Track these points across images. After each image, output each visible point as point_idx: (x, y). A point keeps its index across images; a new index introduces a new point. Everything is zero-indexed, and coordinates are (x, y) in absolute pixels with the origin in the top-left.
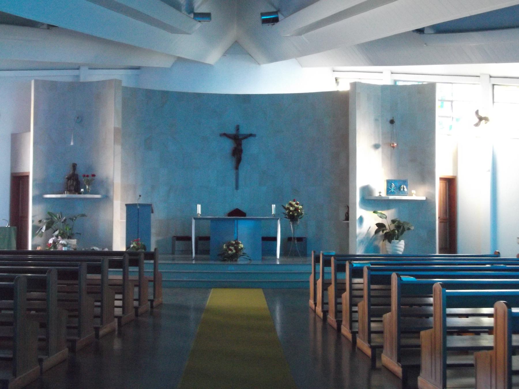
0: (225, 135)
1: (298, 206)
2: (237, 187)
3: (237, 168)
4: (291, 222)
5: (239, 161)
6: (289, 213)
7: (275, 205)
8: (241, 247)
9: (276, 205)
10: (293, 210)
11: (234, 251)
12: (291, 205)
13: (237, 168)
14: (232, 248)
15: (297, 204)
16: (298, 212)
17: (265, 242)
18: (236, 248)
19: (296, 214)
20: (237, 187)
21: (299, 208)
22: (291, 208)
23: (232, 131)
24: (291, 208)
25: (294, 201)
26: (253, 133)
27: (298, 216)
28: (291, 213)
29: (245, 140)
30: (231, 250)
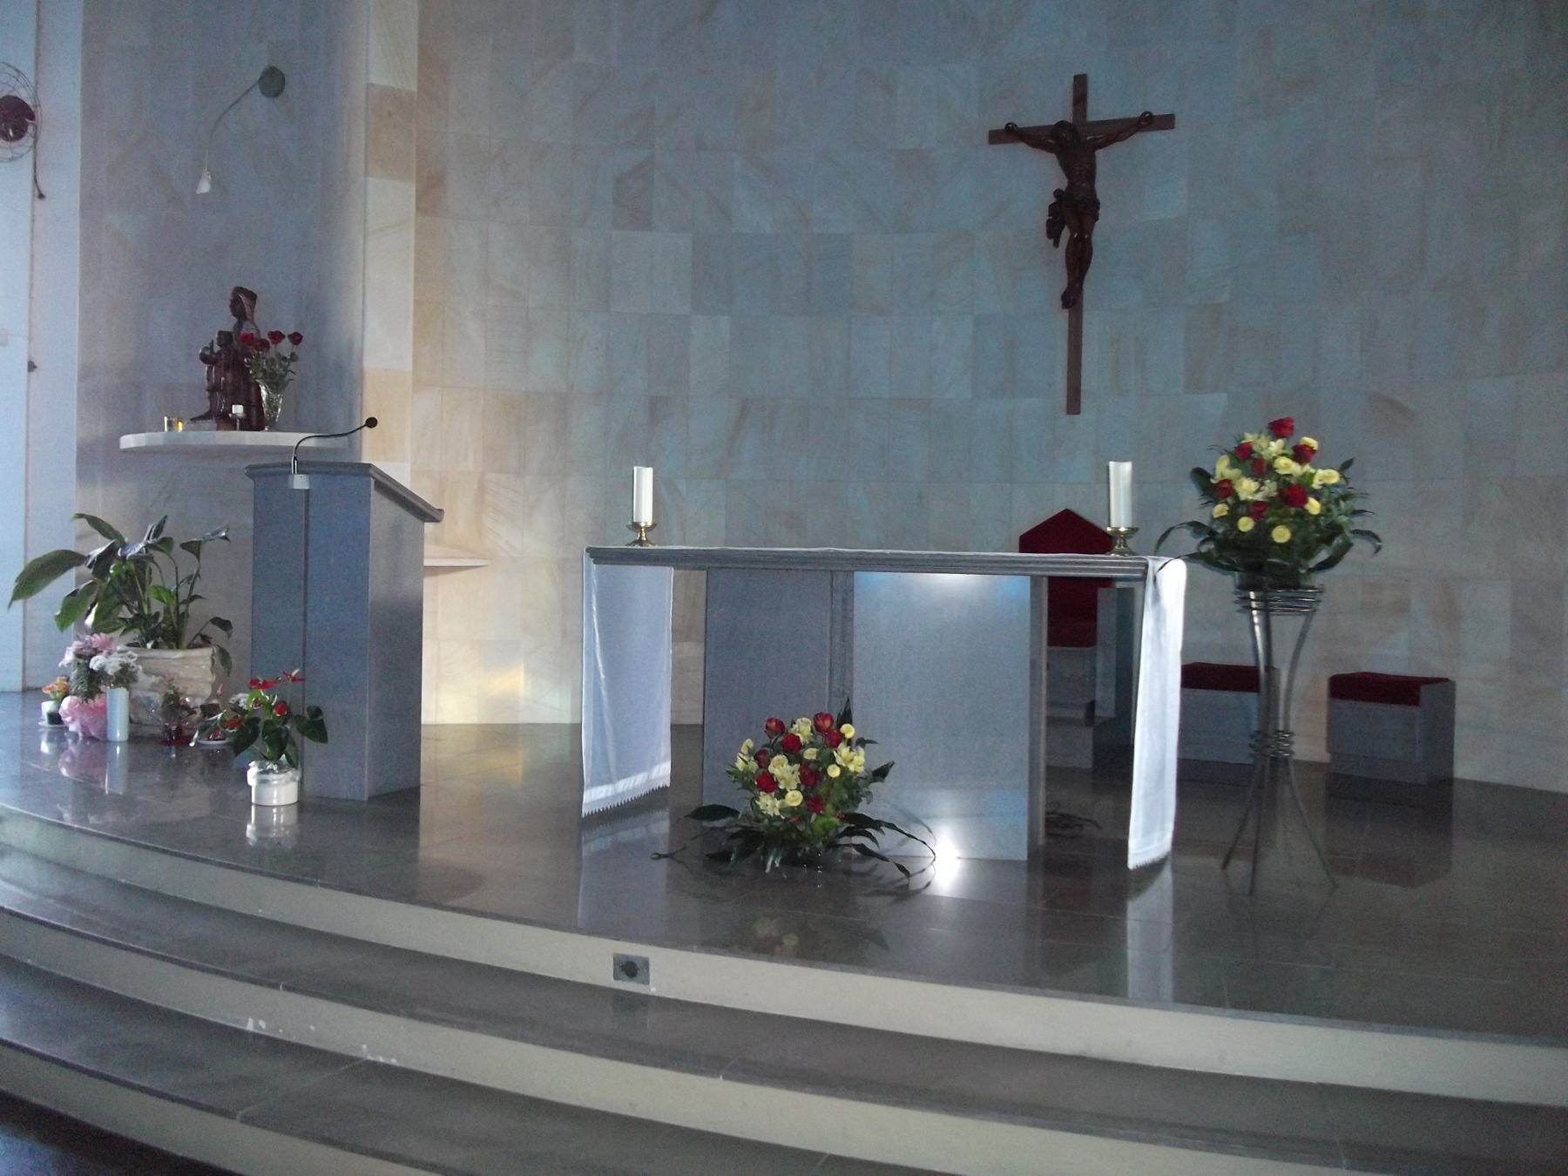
0: (1010, 134)
1: (1307, 468)
2: (1074, 404)
3: (1072, 299)
4: (1252, 595)
5: (1079, 261)
6: (1232, 518)
7: (1127, 467)
8: (844, 770)
9: (1134, 467)
10: (1259, 497)
11: (794, 798)
12: (1245, 457)
13: (1072, 299)
14: (781, 768)
15: (1301, 454)
16: (1304, 514)
17: (1356, 711)
18: (811, 777)
19: (1281, 535)
20: (1074, 404)
21: (1316, 484)
22: (1247, 488)
23: (1052, 109)
24: (1247, 488)
25: (1279, 429)
26: (1158, 110)
27: (1302, 547)
28: (1246, 524)
29: (1117, 149)
30: (769, 784)
